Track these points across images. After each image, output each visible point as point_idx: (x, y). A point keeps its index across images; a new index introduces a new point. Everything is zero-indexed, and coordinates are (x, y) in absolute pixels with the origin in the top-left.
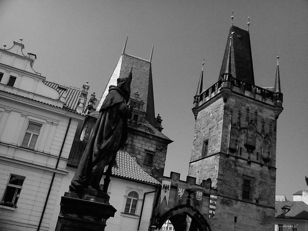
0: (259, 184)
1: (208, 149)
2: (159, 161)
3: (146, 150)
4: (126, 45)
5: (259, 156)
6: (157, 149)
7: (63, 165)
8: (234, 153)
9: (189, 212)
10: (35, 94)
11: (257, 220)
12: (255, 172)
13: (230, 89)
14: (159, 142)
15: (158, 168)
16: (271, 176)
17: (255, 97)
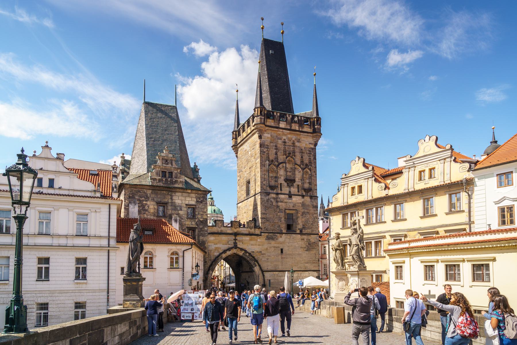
0: (301, 215)
1: (251, 189)
2: (201, 213)
3: (187, 205)
4: (145, 91)
5: (300, 188)
6: (197, 201)
7: (113, 242)
8: (274, 190)
9: (238, 252)
10: (74, 190)
11: (301, 248)
12: (297, 204)
13: (264, 123)
14: (198, 195)
15: (201, 220)
16: (313, 205)
17: (291, 127)
